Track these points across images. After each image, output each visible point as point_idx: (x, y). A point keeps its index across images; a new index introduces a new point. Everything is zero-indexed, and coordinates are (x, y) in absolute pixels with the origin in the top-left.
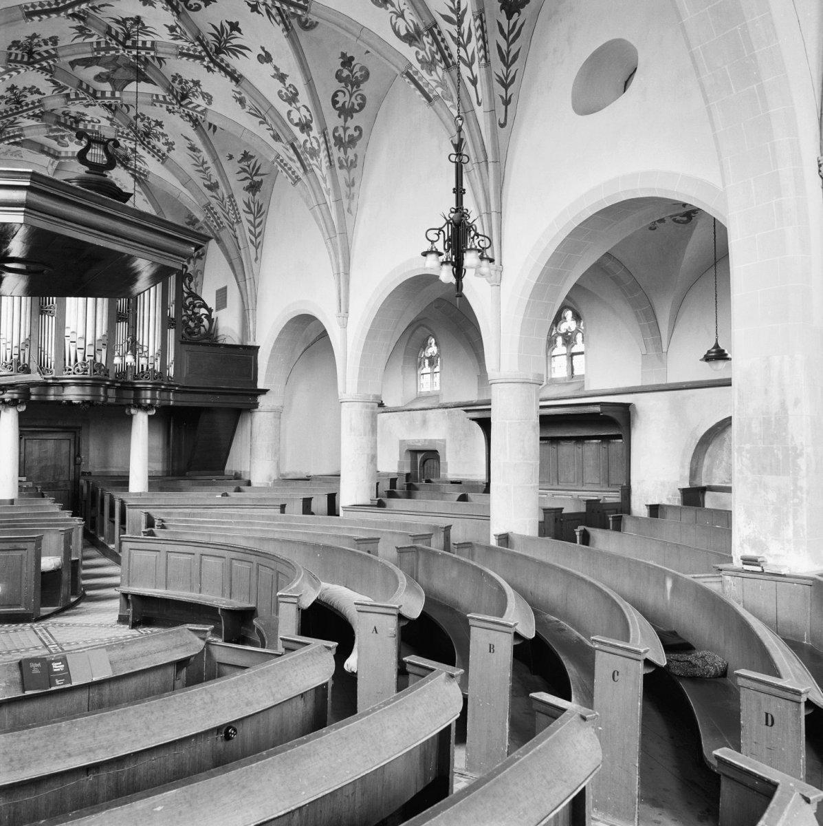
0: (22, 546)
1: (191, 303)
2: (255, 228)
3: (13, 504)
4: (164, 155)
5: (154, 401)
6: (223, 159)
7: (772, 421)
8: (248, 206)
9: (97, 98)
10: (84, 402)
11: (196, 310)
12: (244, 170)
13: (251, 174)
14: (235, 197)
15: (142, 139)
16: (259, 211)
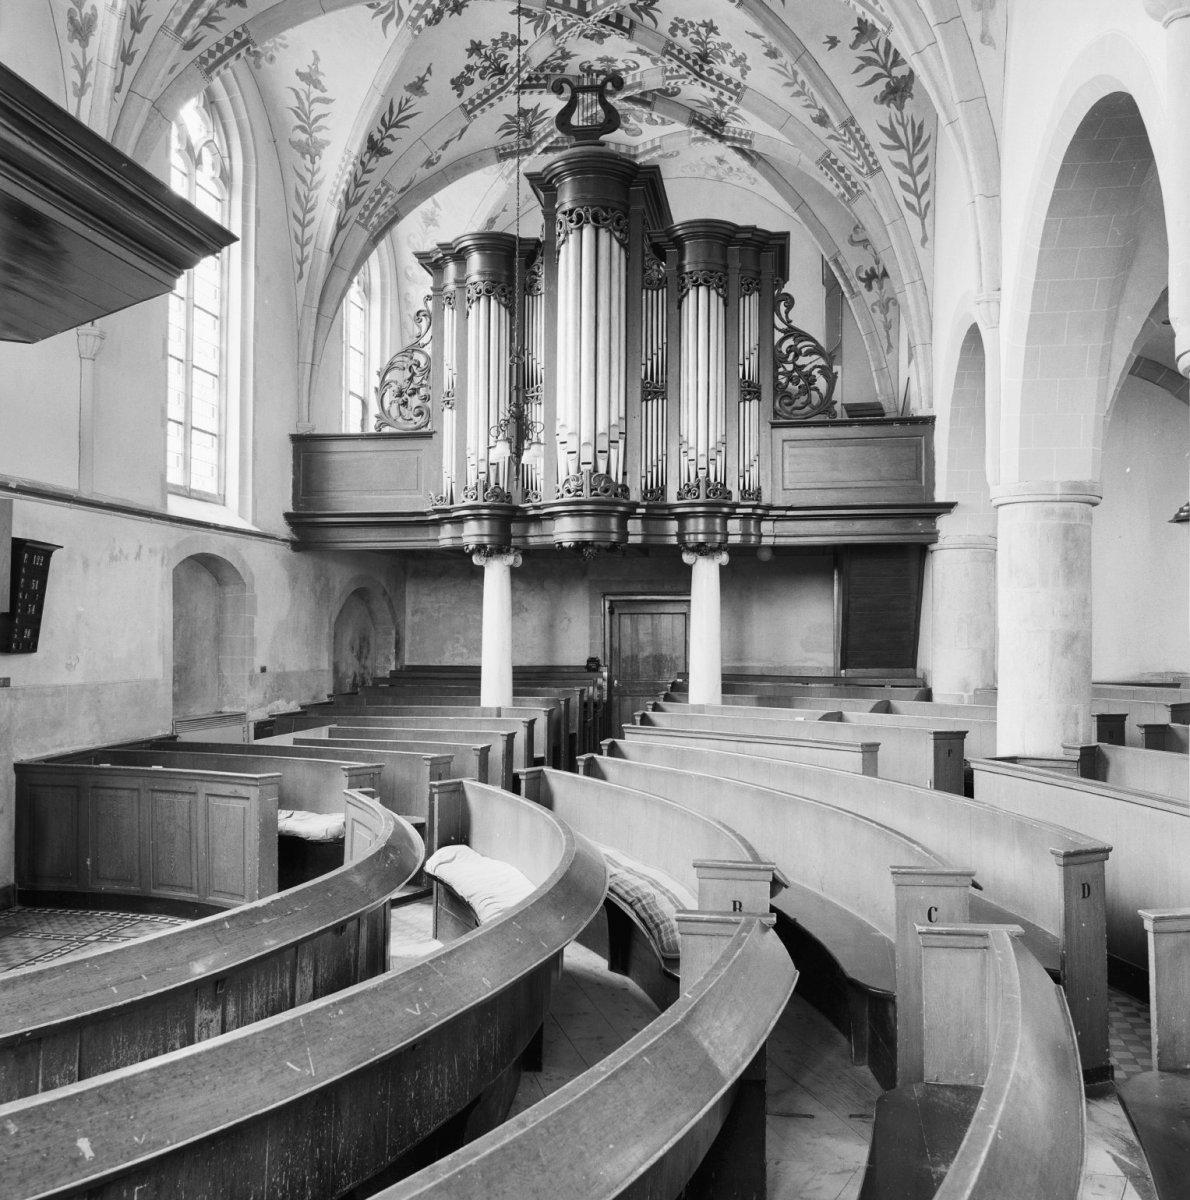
0: (242, 791)
1: (790, 349)
2: (913, 176)
3: (500, 716)
4: (738, 85)
5: (711, 537)
6: (817, 49)
7: (775, 49)
8: (892, 133)
9: (587, 15)
10: (580, 546)
11: (801, 361)
12: (869, 61)
13: (884, 66)
14: (861, 122)
15: (697, 68)
16: (917, 140)
